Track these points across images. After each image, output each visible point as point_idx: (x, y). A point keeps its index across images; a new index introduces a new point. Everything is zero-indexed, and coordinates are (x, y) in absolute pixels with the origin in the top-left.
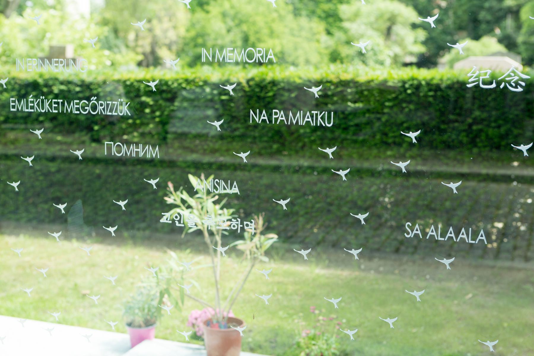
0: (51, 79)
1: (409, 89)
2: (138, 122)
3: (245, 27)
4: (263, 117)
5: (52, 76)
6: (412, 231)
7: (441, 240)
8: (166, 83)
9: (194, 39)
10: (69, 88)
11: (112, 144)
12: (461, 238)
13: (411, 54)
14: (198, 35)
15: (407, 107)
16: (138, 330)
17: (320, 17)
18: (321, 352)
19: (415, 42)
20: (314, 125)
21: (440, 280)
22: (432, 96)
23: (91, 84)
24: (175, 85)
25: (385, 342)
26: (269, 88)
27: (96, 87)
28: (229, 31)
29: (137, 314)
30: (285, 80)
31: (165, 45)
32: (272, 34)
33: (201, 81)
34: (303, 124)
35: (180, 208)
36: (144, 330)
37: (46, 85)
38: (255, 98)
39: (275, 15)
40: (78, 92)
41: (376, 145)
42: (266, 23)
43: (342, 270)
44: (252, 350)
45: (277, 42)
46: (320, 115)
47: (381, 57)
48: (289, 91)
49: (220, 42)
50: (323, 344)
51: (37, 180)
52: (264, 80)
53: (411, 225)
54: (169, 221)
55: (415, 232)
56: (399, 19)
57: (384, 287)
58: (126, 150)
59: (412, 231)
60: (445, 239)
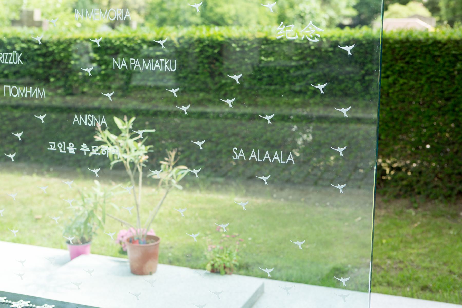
0: (14, 38)
1: (312, 45)
4: (123, 64)
5: (15, 36)
6: (238, 154)
7: (259, 161)
8: (110, 41)
10: (29, 46)
11: (9, 87)
12: (252, 157)
13: (346, 17)
15: (311, 61)
16: (76, 246)
18: (224, 264)
19: (348, 7)
20: (162, 70)
21: (338, 206)
22: (331, 51)
24: (118, 43)
25: (281, 256)
26: (196, 45)
27: (52, 45)
29: (75, 233)
30: (210, 39)
31: (135, 9)
33: (140, 39)
34: (153, 69)
35: (106, 145)
36: (81, 247)
37: (10, 44)
38: (184, 54)
40: (36, 50)
41: (285, 93)
43: (257, 198)
44: (171, 263)
46: (166, 63)
47: (317, 20)
48: (213, 47)
50: (226, 257)
51: (4, 124)
52: (191, 38)
53: (237, 149)
54: (55, 148)
55: (240, 155)
57: (288, 212)
58: (20, 92)
59: (238, 154)
60: (263, 161)
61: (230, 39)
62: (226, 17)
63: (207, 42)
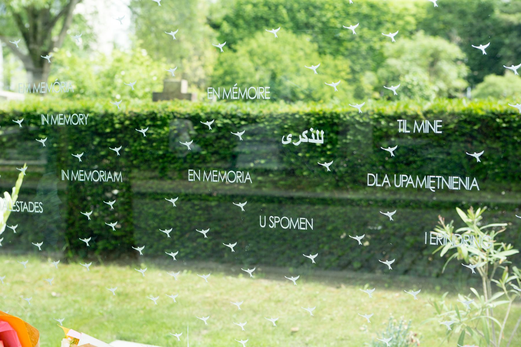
2: (308, 155)
3: (272, 66)
5: (214, 111)
8: (338, 116)
9: (222, 77)
14: (226, 73)
23: (257, 117)
28: (256, 70)
30: (466, 112)
31: (195, 83)
39: (301, 53)
42: (292, 61)
45: (303, 79)
47: (427, 93)
49: (248, 80)
56: (443, 55)
61: (493, 113)
62: (298, 90)
63: (464, 117)
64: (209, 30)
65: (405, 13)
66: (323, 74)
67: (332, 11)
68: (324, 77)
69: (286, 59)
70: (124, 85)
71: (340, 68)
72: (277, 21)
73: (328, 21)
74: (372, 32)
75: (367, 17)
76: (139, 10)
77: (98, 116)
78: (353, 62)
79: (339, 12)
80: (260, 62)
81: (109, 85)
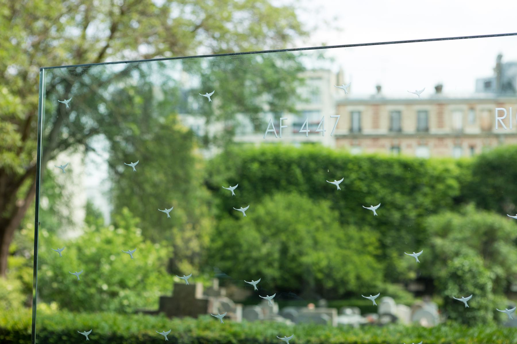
3: (283, 237)
9: (220, 250)
14: (226, 246)
17: (370, 225)
32: (316, 244)
42: (309, 232)
45: (322, 255)
47: (482, 280)
64: (206, 193)
65: (446, 175)
66: (345, 248)
67: (357, 171)
68: (347, 252)
69: (302, 229)
70: (113, 272)
71: (367, 241)
72: (289, 182)
73: (352, 182)
74: (406, 198)
75: (399, 179)
76: (121, 169)
77: (103, 339)
78: (383, 234)
79: (365, 173)
80: (267, 233)
81: (93, 271)
